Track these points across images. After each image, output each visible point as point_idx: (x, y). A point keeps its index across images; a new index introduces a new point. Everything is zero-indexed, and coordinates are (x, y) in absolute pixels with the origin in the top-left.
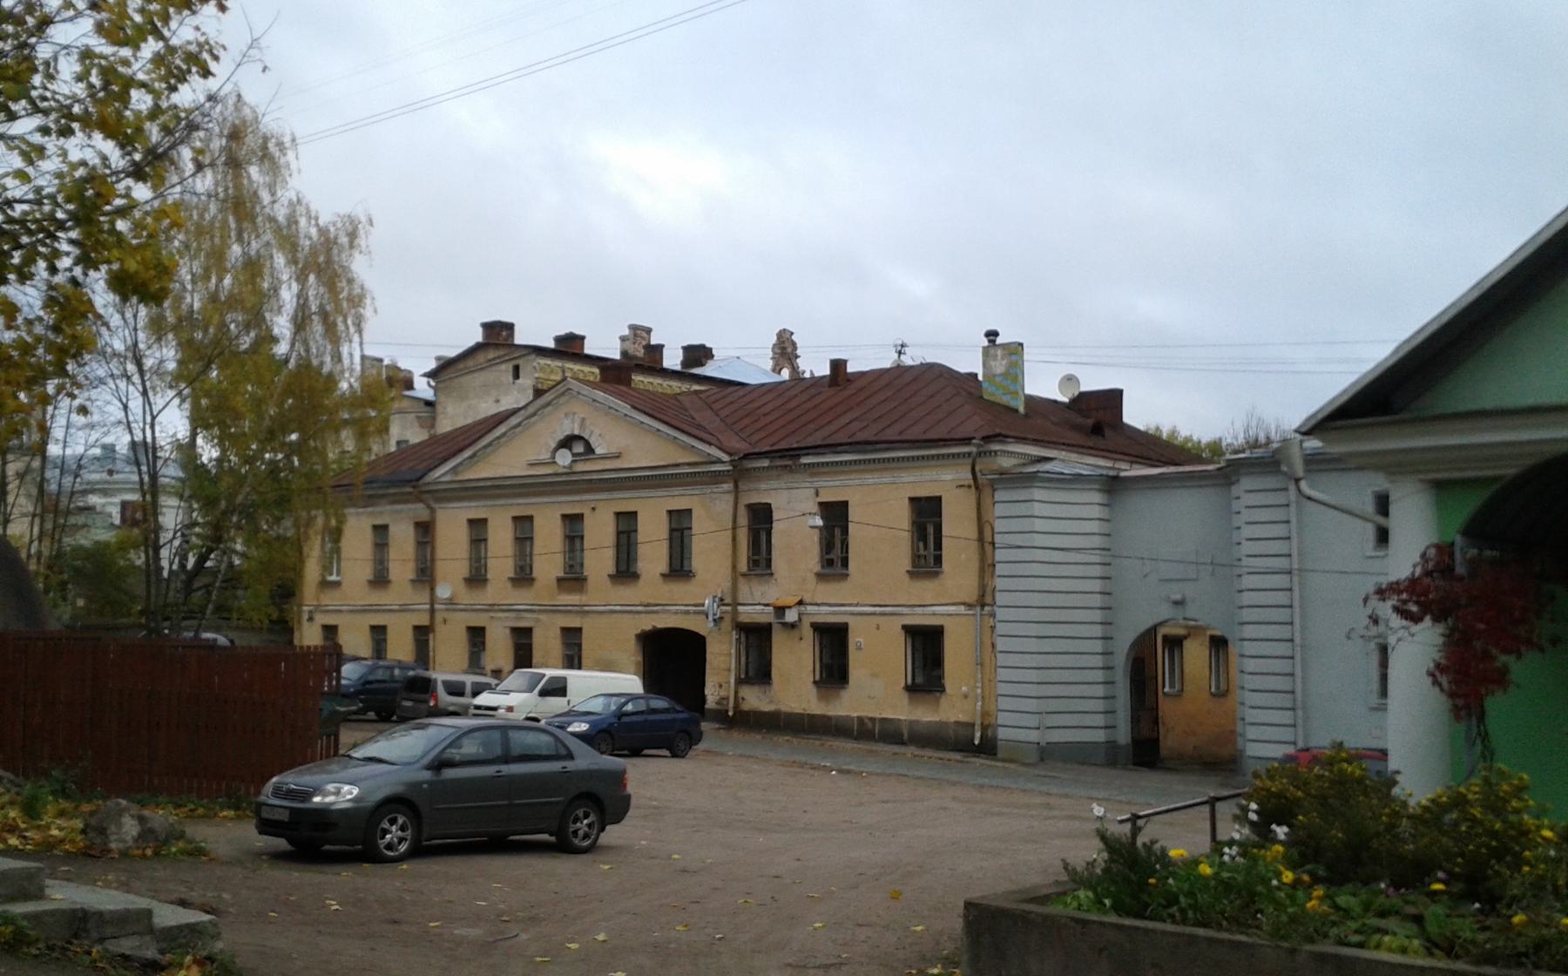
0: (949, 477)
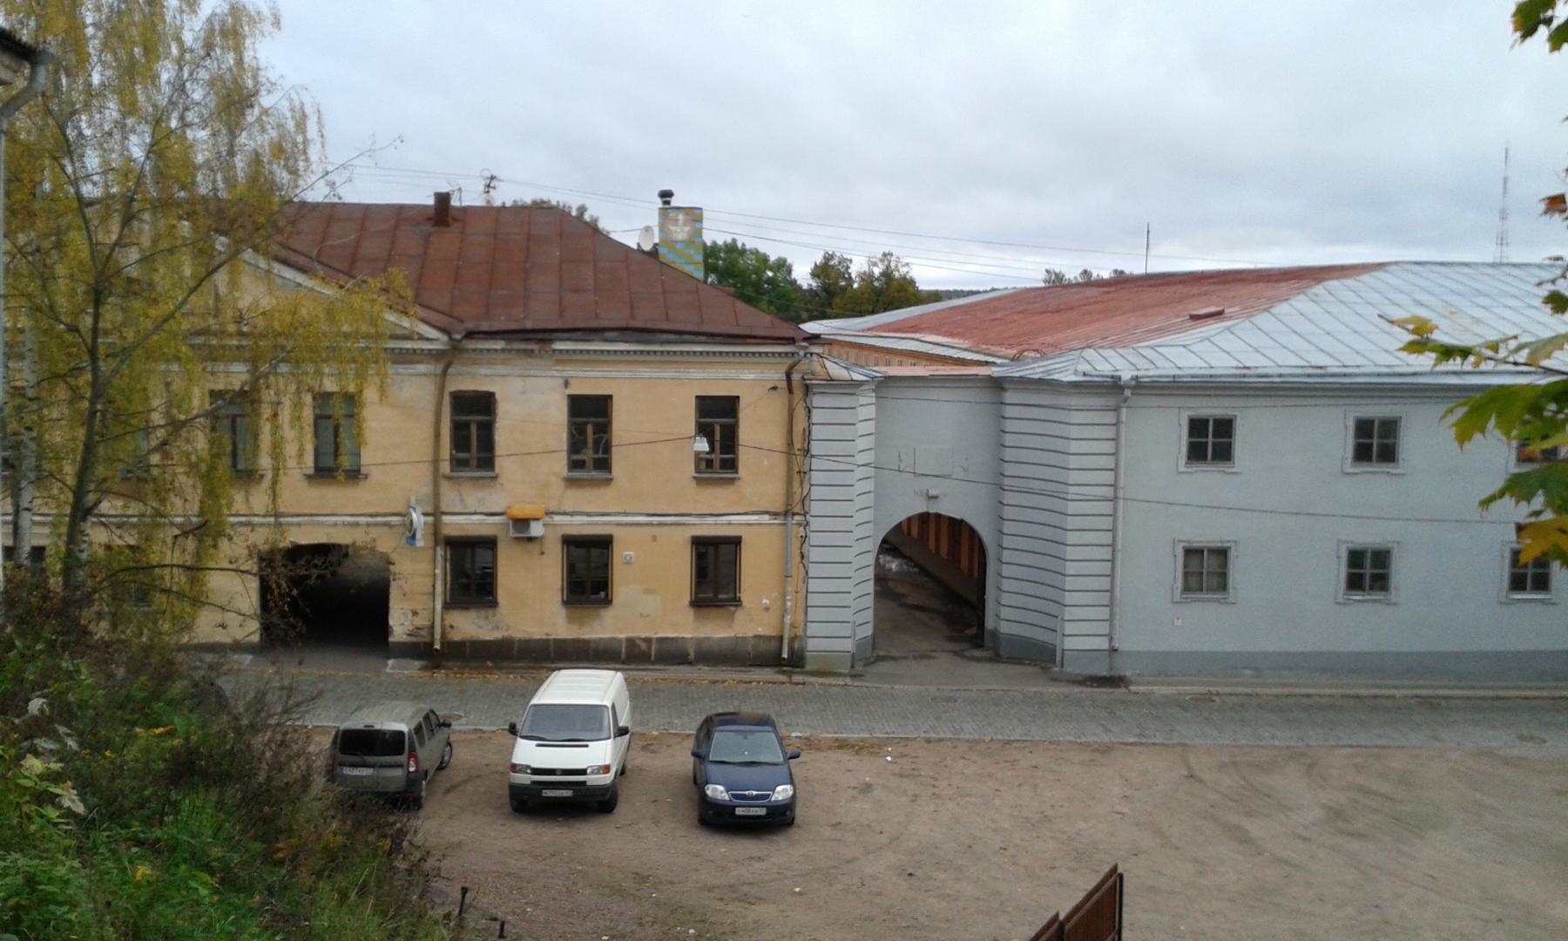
0: (751, 376)
